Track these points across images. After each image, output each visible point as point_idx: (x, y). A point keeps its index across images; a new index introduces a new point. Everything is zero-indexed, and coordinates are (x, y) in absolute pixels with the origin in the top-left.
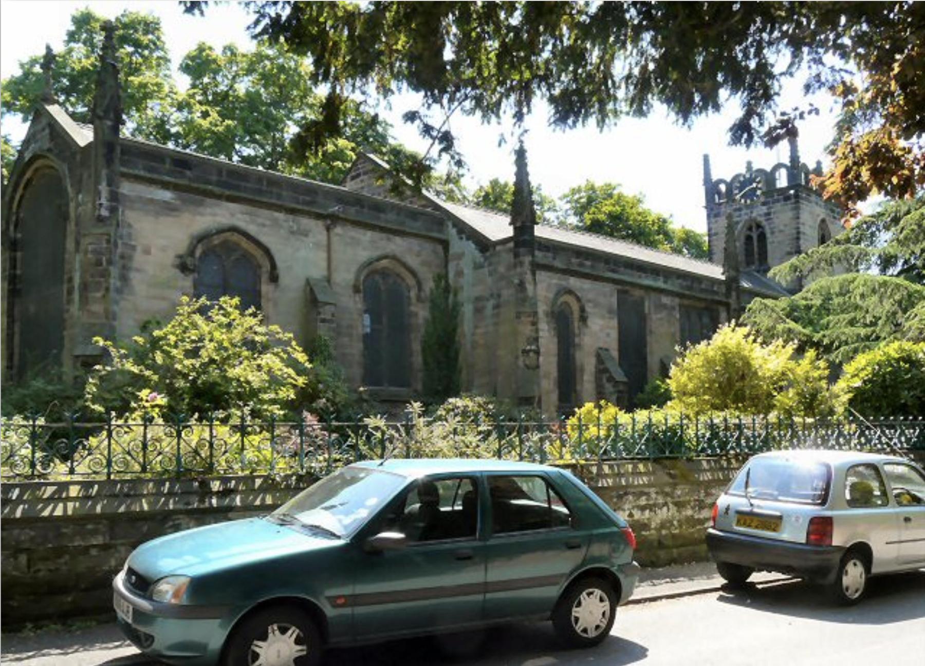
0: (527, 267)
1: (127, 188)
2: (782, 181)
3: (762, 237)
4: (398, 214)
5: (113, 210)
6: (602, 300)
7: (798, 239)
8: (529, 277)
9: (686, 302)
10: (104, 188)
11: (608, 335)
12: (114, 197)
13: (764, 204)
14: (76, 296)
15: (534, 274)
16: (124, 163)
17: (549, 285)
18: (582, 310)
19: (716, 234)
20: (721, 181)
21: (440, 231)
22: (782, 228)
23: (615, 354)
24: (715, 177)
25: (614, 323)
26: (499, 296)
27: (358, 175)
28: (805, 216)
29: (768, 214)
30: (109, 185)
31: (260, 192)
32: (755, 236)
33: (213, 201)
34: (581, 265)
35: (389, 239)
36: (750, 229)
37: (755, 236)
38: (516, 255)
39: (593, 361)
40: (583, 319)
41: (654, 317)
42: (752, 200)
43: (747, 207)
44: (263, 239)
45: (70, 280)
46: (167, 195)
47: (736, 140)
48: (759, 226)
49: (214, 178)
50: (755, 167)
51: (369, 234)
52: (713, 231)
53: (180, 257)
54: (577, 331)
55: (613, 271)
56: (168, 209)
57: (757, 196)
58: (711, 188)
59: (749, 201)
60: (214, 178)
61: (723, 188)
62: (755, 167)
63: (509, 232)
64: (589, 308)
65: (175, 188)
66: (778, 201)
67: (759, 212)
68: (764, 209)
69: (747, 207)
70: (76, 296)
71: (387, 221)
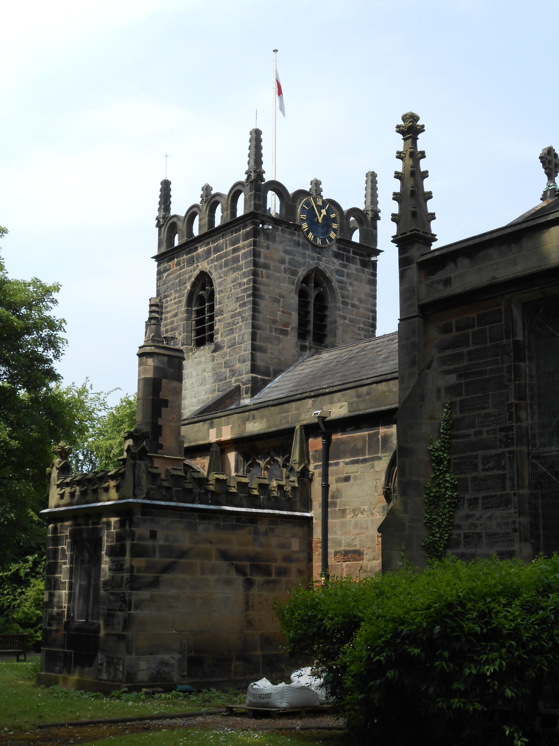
13: (337, 255)
22: (357, 303)
32: (313, 294)
37: (313, 294)
42: (323, 241)
52: (262, 260)
57: (331, 240)
58: (167, 224)
59: (319, 241)
67: (330, 265)
68: (337, 262)
69: (315, 247)
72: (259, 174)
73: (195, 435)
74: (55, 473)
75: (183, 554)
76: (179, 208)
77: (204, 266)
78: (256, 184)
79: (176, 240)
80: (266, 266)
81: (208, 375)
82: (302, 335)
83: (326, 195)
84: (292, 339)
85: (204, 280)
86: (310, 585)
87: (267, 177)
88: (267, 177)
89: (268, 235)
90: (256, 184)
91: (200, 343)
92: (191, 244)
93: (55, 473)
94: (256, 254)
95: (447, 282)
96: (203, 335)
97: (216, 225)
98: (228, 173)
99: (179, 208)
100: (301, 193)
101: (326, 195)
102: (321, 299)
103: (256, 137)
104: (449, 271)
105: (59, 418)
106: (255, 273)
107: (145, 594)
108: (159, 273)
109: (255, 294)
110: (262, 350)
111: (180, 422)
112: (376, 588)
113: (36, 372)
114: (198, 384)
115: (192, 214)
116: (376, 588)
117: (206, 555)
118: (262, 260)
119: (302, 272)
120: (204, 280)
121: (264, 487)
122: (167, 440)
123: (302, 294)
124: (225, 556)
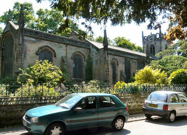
0: (106, 54)
1: (25, 38)
2: (158, 36)
3: (154, 48)
4: (80, 43)
5: (23, 42)
6: (121, 61)
7: (161, 48)
8: (107, 56)
9: (138, 61)
10: (21, 38)
11: (123, 68)
12: (23, 40)
13: (154, 41)
14: (15, 60)
15: (108, 55)
16: (25, 33)
17: (111, 58)
18: (118, 63)
19: (144, 47)
20: (145, 37)
21: (89, 47)
23: (124, 72)
24: (144, 36)
25: (124, 65)
26: (101, 60)
27: (72, 35)
28: (162, 44)
29: (155, 43)
30: (22, 37)
31: (52, 39)
33: (43, 41)
34: (117, 54)
35: (78, 48)
36: (151, 46)
38: (104, 52)
39: (120, 73)
40: (118, 65)
41: (132, 64)
43: (151, 42)
44: (53, 48)
45: (14, 56)
46: (34, 39)
47: (148, 28)
48: (153, 46)
49: (43, 36)
50: (152, 34)
51: (74, 47)
53: (36, 52)
54: (116, 67)
55: (124, 55)
56: (34, 42)
58: (144, 38)
60: (43, 36)
61: (146, 38)
62: (152, 34)
63: (103, 47)
64: (119, 62)
65: (35, 38)
66: (157, 41)
69: (151, 42)
70: (15, 60)
71: (78, 45)
80: (144, 47)
103: (142, 32)
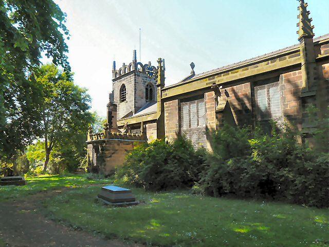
52: (136, 81)
69: (149, 78)
72: (136, 60)
73: (119, 124)
74: (89, 133)
75: (117, 150)
76: (117, 69)
77: (123, 82)
78: (136, 63)
79: (118, 76)
81: (125, 108)
82: (147, 98)
83: (152, 65)
84: (144, 100)
85: (123, 86)
86: (4, 93)
87: (138, 61)
88: (138, 61)
89: (138, 76)
90: (136, 63)
91: (123, 101)
92: (120, 78)
93: (89, 133)
94: (135, 80)
95: (166, 95)
96: (123, 99)
97: (126, 72)
98: (129, 60)
99: (117, 69)
100: (146, 65)
101: (152, 65)
102: (151, 90)
104: (167, 92)
105: (90, 119)
106: (135, 85)
107: (109, 159)
108: (113, 84)
109: (135, 89)
110: (137, 102)
111: (116, 121)
112: (274, 199)
113: (85, 107)
114: (123, 109)
115: (120, 70)
116: (274, 199)
117: (122, 151)
118: (136, 81)
119: (146, 84)
120: (123, 86)
121: (135, 136)
122: (113, 125)
123: (147, 89)
124: (173, 171)
